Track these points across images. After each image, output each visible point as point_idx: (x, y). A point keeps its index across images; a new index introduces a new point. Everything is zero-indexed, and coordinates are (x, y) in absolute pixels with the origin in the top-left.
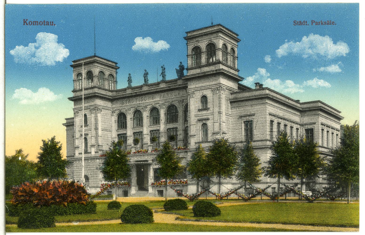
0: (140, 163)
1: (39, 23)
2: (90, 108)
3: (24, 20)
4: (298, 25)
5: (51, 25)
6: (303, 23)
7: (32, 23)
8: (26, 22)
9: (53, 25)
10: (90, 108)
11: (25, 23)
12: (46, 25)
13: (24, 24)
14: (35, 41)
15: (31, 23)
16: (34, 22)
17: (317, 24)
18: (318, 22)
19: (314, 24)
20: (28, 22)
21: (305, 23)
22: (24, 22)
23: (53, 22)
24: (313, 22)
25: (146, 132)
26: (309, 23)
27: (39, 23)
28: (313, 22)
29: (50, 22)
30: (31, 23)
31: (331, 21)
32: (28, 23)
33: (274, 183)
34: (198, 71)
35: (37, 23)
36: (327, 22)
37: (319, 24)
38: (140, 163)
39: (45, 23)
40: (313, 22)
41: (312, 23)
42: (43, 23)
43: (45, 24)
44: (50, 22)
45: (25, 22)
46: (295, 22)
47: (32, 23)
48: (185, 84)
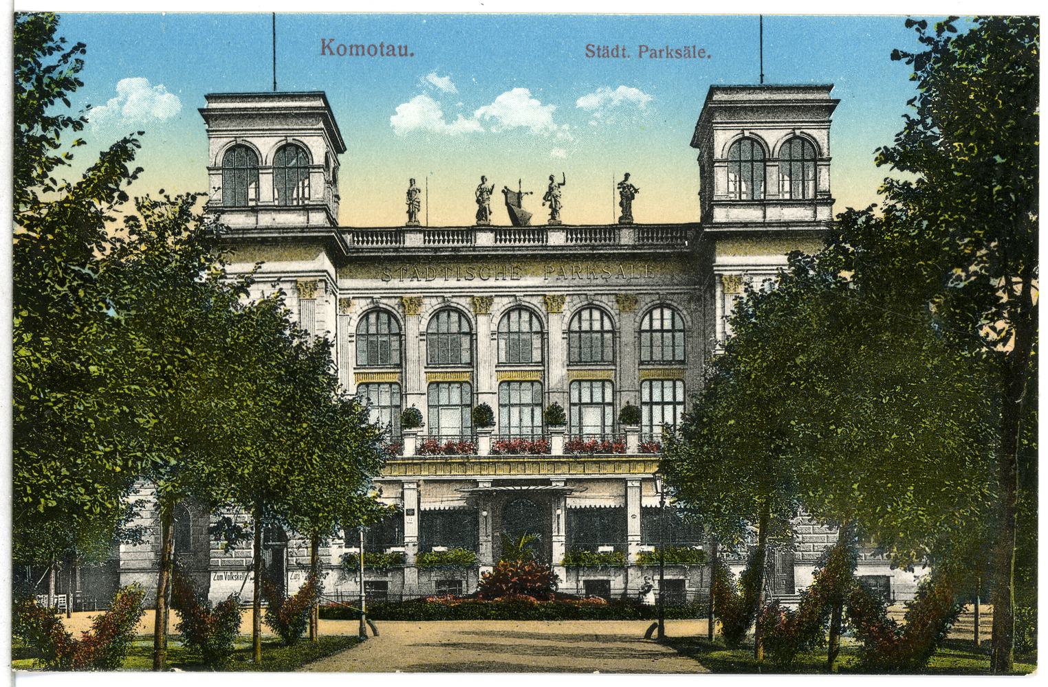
0: (511, 488)
1: (366, 48)
2: (299, 279)
3: (323, 41)
4: (382, 55)
5: (401, 55)
6: (615, 53)
7: (345, 49)
8: (328, 46)
9: (406, 54)
10: (299, 279)
11: (327, 51)
12: (388, 54)
13: (323, 53)
14: (115, 94)
15: (342, 49)
16: (351, 47)
17: (654, 55)
18: (349, 44)
19: (646, 55)
20: (334, 46)
21: (621, 52)
22: (323, 48)
23: (406, 47)
24: (644, 49)
25: (487, 385)
26: (633, 51)
27: (366, 48)
28: (642, 49)
29: (400, 47)
30: (342, 49)
31: (694, 47)
32: (335, 51)
33: (142, 570)
34: (754, 214)
35: (360, 48)
36: (683, 49)
37: (661, 56)
38: (511, 488)
39: (385, 51)
40: (642, 49)
41: (641, 52)
42: (379, 49)
43: (385, 53)
44: (400, 47)
45: (325, 47)
46: (590, 47)
47: (345, 49)
48: (594, 246)
